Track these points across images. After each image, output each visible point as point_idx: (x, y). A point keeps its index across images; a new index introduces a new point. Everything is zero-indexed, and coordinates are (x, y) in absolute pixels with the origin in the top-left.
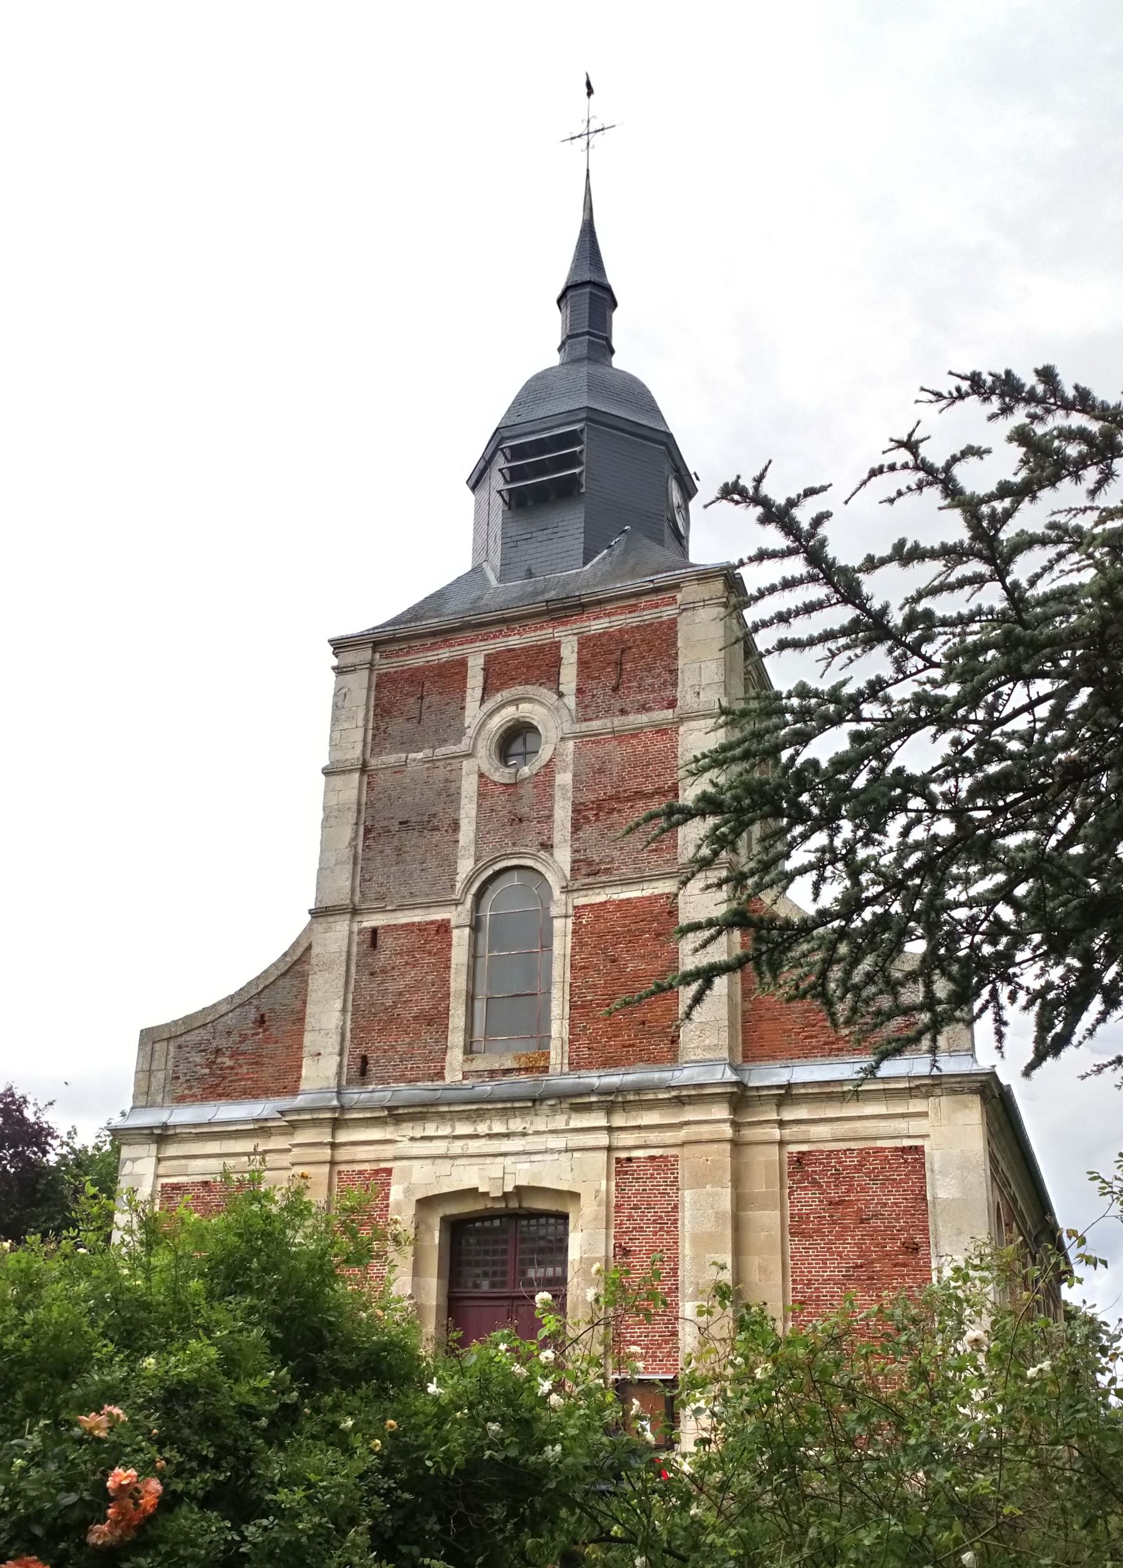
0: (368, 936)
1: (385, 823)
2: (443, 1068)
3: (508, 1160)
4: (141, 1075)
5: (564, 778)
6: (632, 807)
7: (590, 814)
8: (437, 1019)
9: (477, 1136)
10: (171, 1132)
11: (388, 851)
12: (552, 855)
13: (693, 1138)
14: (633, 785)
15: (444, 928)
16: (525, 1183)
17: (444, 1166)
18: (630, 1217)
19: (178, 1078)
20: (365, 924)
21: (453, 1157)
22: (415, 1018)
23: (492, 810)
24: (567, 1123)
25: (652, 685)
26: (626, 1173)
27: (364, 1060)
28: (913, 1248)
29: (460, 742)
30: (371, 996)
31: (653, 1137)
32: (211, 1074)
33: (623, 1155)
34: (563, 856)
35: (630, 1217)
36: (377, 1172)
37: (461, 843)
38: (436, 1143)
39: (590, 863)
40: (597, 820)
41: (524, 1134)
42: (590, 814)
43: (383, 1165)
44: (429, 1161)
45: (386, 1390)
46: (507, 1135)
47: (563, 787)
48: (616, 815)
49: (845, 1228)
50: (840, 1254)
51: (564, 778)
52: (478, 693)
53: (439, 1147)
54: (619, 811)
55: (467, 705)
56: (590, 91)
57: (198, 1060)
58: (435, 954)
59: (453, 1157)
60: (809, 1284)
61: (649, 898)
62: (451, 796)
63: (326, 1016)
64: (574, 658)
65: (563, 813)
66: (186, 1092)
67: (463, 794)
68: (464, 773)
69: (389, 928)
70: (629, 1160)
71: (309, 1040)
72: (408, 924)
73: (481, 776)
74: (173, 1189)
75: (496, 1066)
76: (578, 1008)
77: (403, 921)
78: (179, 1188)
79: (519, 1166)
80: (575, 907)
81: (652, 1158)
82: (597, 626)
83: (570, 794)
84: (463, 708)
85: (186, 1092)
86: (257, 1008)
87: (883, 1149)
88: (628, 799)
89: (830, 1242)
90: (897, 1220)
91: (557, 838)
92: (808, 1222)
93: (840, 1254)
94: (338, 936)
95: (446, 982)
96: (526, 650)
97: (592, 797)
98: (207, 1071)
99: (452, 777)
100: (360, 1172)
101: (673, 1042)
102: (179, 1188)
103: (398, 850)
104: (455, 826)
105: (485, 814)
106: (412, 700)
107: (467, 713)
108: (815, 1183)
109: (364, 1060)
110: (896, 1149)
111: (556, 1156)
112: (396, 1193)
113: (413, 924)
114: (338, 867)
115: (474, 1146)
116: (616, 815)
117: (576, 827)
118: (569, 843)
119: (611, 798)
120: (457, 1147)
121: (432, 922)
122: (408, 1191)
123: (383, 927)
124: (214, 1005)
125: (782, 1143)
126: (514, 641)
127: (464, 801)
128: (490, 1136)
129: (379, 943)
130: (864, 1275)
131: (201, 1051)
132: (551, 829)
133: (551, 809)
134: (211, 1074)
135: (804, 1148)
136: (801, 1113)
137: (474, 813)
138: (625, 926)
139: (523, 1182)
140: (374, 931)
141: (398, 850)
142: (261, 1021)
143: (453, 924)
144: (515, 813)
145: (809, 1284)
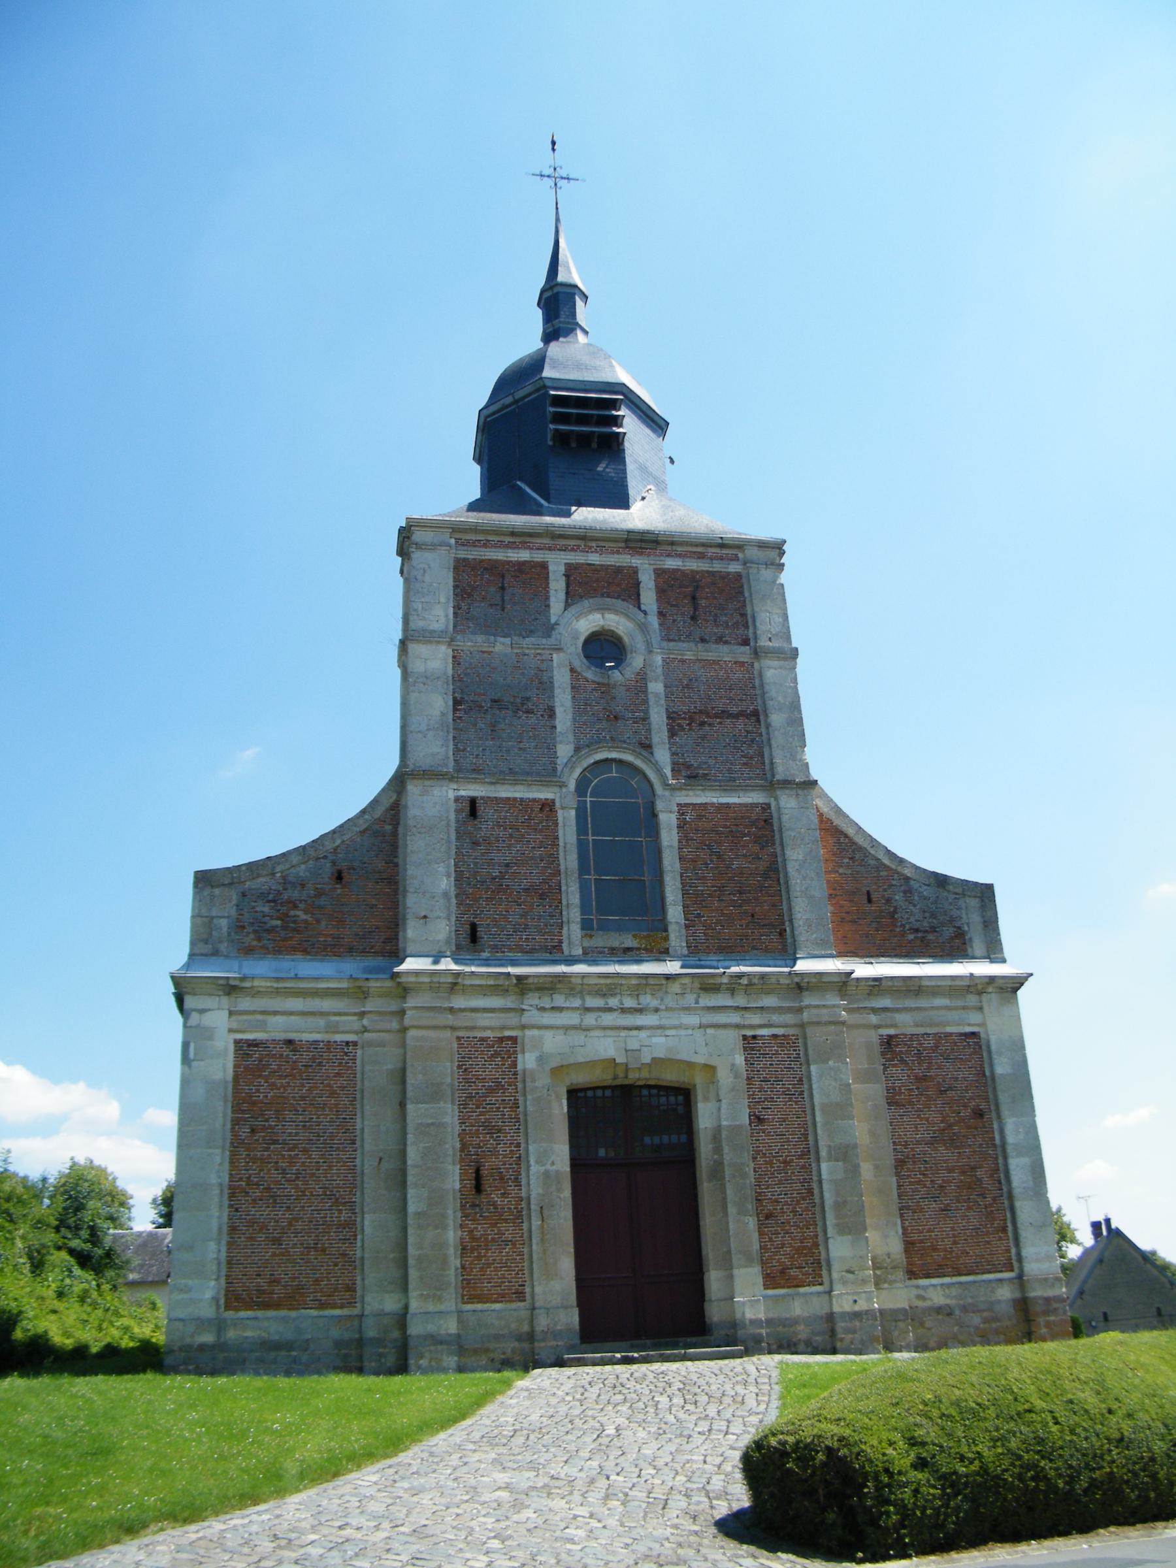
0: (467, 805)
1: (476, 698)
2: (561, 942)
3: (643, 1034)
4: (199, 921)
5: (656, 687)
6: (720, 723)
7: (684, 723)
8: (549, 893)
9: (610, 1010)
10: (247, 984)
11: (481, 725)
12: (652, 753)
13: (815, 1020)
14: (720, 705)
15: (548, 807)
16: (661, 1055)
17: (578, 1038)
18: (761, 1089)
19: (243, 927)
20: (463, 793)
21: (587, 1029)
22: (526, 890)
23: (586, 704)
24: (697, 1002)
25: (727, 623)
26: (753, 1049)
27: (474, 928)
28: (979, 1114)
29: (550, 637)
30: (476, 864)
31: (775, 1018)
32: (284, 928)
33: (749, 1033)
34: (663, 755)
35: (761, 1089)
36: (501, 1040)
37: (559, 729)
38: (565, 1014)
39: (689, 767)
40: (690, 729)
41: (657, 1010)
42: (684, 723)
43: (507, 1033)
44: (561, 1032)
45: (1066, 1483)
46: (640, 1011)
47: (657, 695)
48: (707, 728)
49: (929, 1098)
50: (927, 1119)
51: (656, 687)
52: (562, 596)
53: (573, 1019)
54: (710, 725)
55: (552, 604)
56: (554, 143)
57: (266, 910)
58: (541, 831)
59: (587, 1029)
60: (906, 1145)
61: (746, 805)
62: (546, 687)
63: (431, 881)
64: (652, 585)
65: (658, 717)
66: (255, 943)
67: (556, 685)
68: (555, 665)
69: (488, 800)
70: (754, 1037)
71: (413, 902)
72: (508, 799)
73: (572, 670)
74: (249, 1045)
75: (616, 944)
76: (691, 898)
77: (504, 795)
78: (256, 1045)
79: (655, 1040)
80: (678, 805)
81: (775, 1036)
82: (671, 563)
83: (663, 702)
84: (548, 606)
85: (255, 943)
86: (334, 863)
87: (951, 1034)
88: (716, 716)
89: (919, 1110)
90: (967, 1091)
91: (655, 739)
92: (900, 1093)
93: (927, 1119)
94: (434, 804)
95: (553, 859)
96: (604, 568)
97: (684, 708)
98: (279, 923)
99: (544, 666)
100: (482, 1039)
101: (780, 934)
102: (256, 1045)
103: (493, 727)
104: (551, 713)
105: (581, 707)
106: (492, 589)
107: (552, 611)
108: (902, 1061)
109: (474, 928)
110: (961, 1034)
111: (690, 1032)
112: (527, 1061)
113: (515, 799)
114: (431, 733)
115: (608, 1019)
116: (707, 728)
117: (672, 733)
118: (667, 746)
119: (701, 712)
120: (590, 1019)
121: (534, 800)
122: (540, 1059)
123: (482, 798)
124: (284, 855)
125: (877, 1027)
126: (595, 559)
127: (557, 691)
128: (624, 1010)
129: (479, 813)
130: (946, 1137)
131: (269, 901)
132: (649, 730)
133: (646, 712)
134: (284, 928)
135: (892, 1032)
136: (886, 1002)
137: (569, 703)
138: (725, 827)
139: (661, 1054)
140: (473, 802)
141: (493, 727)
142: (339, 877)
143: (558, 804)
144: (610, 714)
145: (906, 1145)
